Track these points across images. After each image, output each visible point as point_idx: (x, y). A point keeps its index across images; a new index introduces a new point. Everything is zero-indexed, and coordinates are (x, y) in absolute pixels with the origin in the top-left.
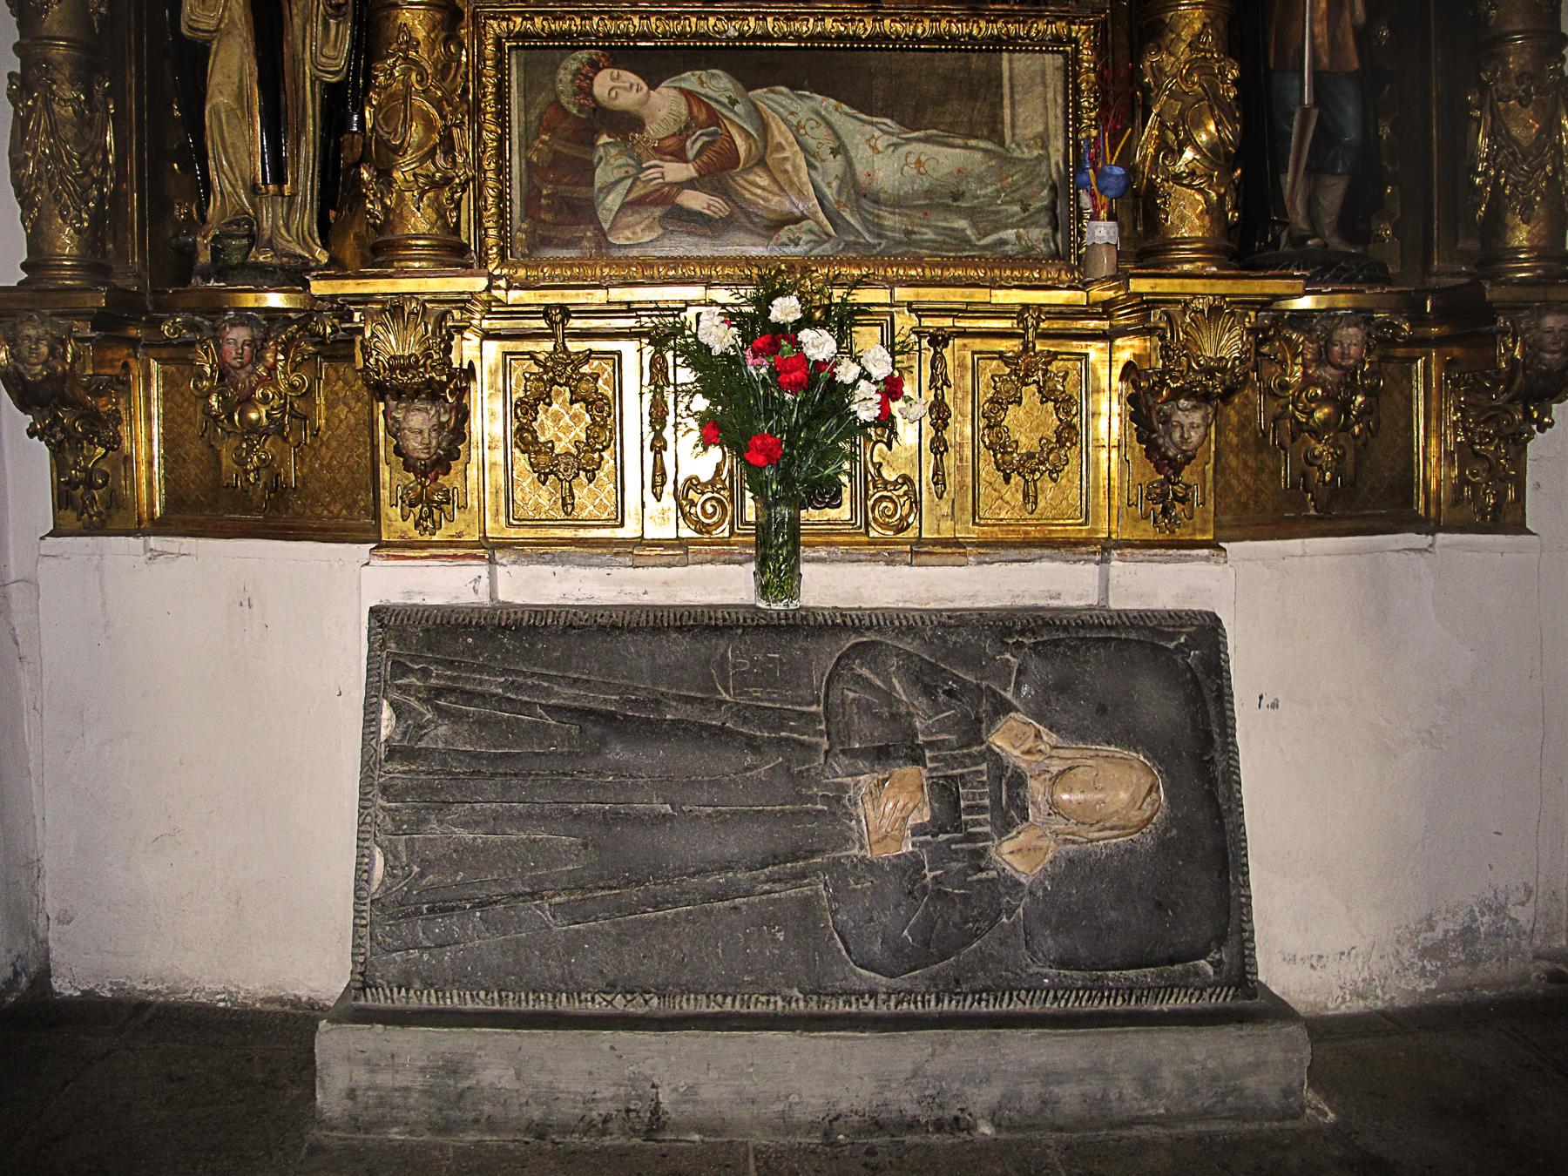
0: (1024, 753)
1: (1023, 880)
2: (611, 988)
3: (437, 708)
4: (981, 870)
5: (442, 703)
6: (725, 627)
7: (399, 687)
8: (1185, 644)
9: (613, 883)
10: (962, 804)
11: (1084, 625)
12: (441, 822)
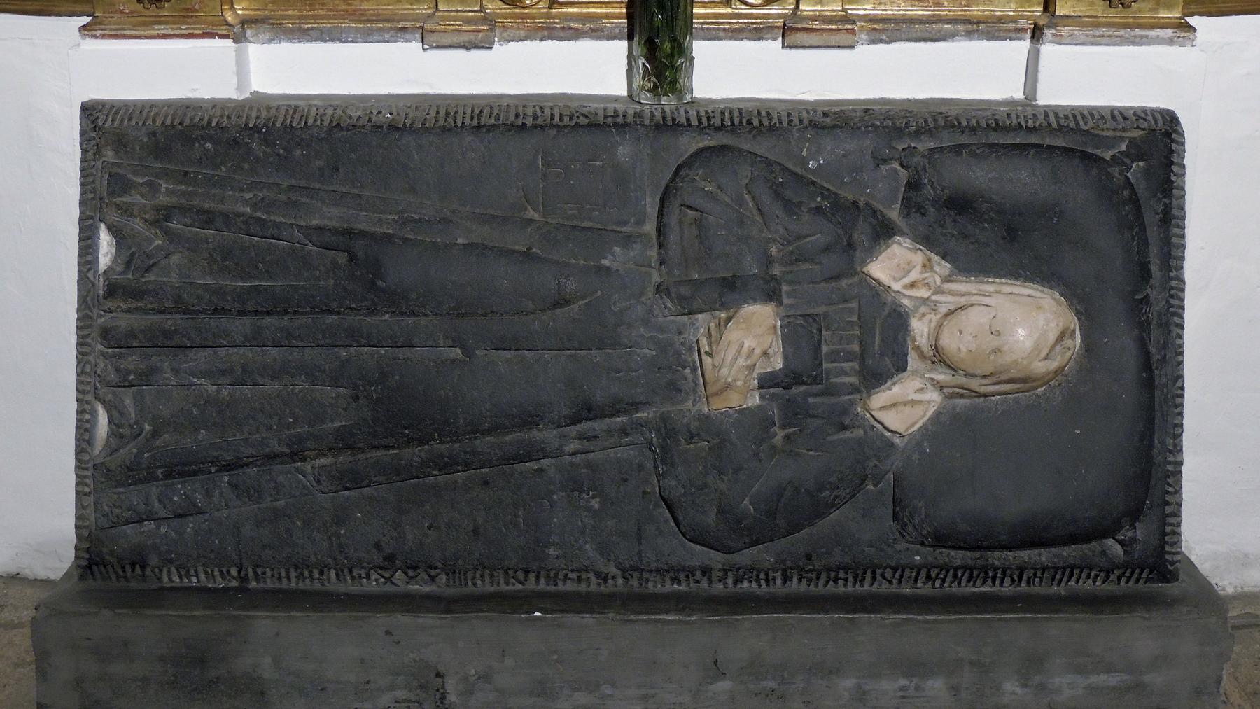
0: (905, 287)
1: (897, 440)
2: (390, 560)
3: (167, 233)
4: (845, 428)
5: (174, 225)
6: (535, 126)
7: (118, 207)
8: (1127, 154)
9: (391, 441)
10: (825, 349)
11: (997, 127)
12: (176, 371)
